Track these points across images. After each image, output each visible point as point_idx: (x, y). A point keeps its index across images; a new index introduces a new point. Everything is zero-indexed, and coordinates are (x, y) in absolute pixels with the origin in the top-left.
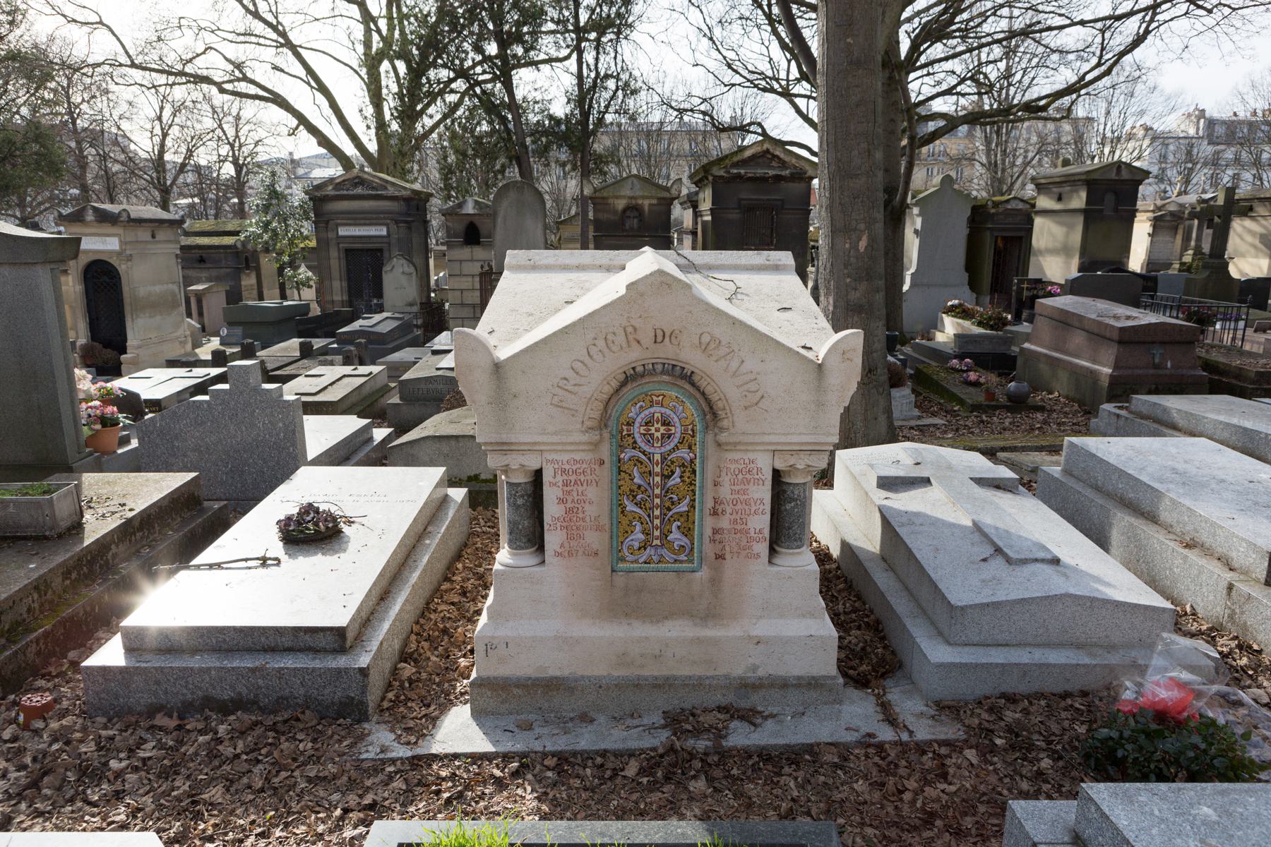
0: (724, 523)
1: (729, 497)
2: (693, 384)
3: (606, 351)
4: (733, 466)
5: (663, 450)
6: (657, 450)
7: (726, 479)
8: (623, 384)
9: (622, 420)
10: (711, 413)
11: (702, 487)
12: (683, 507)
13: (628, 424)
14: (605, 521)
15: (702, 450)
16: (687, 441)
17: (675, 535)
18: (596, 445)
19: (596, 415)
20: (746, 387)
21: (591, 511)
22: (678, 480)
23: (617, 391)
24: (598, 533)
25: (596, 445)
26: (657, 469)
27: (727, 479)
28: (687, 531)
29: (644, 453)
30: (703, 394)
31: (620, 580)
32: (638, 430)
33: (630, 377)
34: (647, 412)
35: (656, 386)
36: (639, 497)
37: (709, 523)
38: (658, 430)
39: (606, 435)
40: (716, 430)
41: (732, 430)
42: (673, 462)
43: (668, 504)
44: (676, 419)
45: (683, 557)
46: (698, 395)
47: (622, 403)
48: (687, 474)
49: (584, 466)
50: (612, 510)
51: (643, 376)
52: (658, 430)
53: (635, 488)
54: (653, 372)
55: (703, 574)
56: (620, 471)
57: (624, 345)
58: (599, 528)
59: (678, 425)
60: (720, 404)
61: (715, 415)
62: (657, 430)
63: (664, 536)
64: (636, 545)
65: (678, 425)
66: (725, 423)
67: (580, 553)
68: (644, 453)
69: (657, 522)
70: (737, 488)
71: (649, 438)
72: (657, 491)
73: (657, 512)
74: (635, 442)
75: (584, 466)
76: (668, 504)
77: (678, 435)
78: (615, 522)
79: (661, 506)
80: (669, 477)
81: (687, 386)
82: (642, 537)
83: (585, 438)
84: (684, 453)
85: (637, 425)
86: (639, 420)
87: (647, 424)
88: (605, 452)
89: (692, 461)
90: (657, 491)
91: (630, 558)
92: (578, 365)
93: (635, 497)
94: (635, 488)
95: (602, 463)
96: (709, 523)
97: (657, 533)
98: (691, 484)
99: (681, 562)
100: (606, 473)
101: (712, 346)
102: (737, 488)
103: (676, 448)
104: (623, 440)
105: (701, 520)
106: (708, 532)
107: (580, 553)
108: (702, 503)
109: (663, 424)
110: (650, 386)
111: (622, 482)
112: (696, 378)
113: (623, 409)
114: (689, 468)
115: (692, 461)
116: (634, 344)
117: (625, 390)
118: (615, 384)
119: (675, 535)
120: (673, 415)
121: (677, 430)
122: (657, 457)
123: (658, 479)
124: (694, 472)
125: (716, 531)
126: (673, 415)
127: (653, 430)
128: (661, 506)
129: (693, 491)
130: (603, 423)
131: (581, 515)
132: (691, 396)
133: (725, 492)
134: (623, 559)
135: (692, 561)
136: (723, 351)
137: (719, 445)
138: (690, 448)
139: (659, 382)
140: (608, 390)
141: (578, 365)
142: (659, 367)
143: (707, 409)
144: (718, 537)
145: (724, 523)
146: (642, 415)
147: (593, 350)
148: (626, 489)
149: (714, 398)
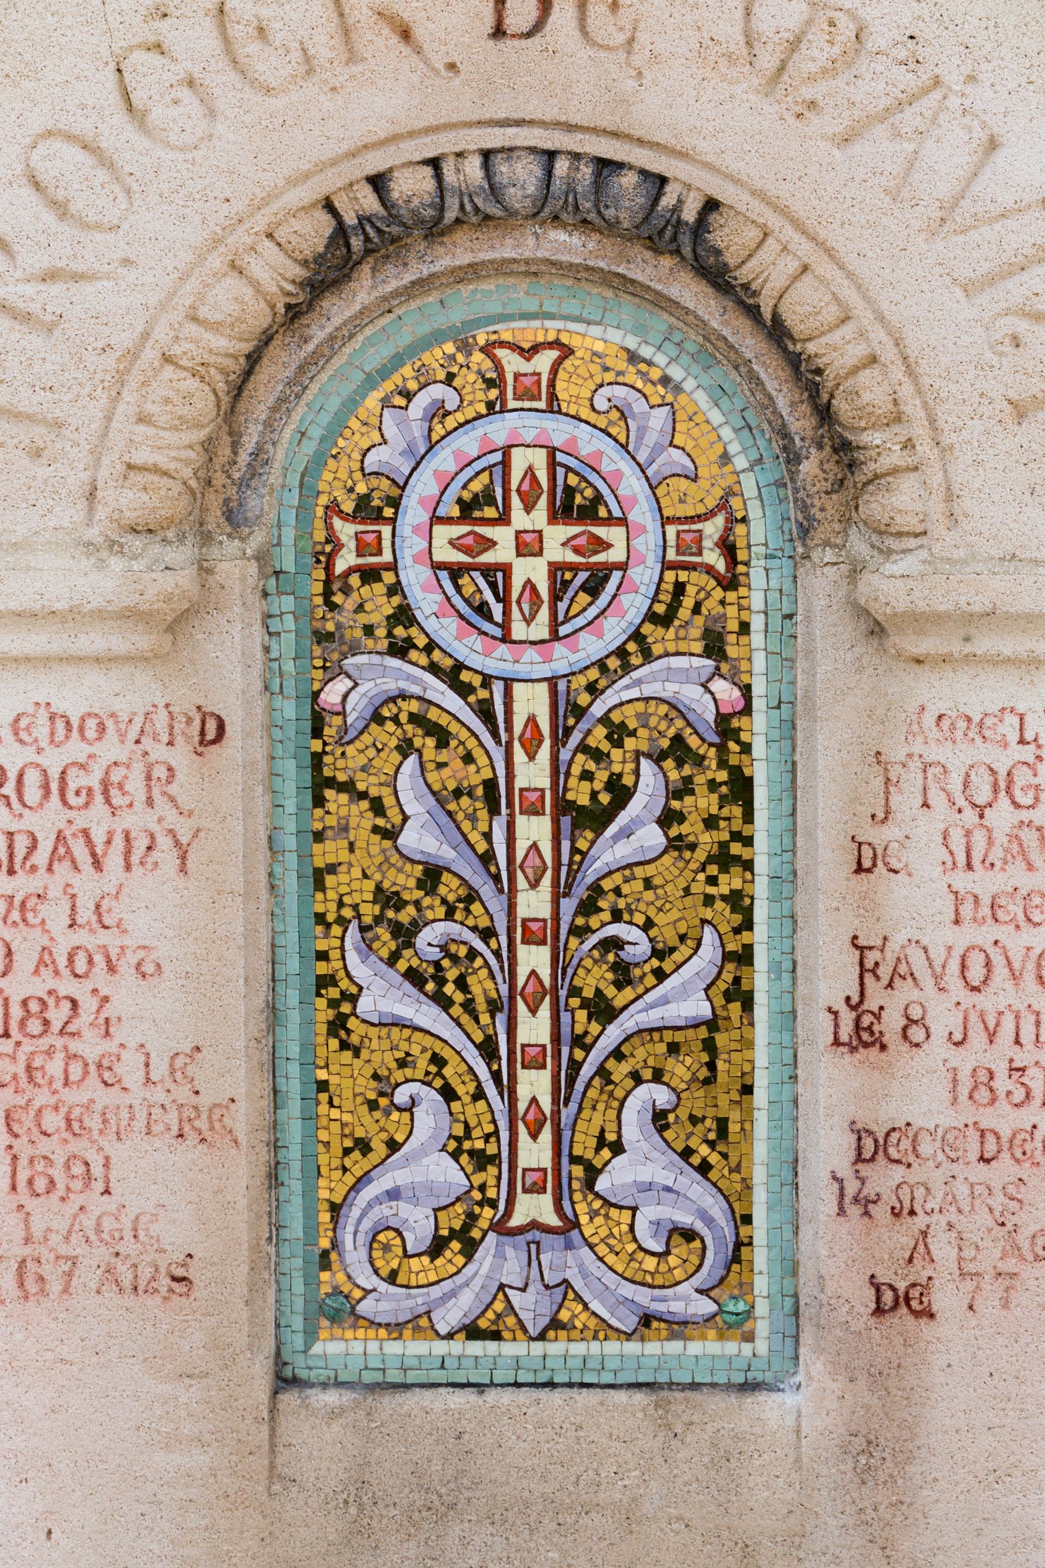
0: (918, 1092)
1: (943, 938)
2: (716, 275)
3: (221, 80)
4: (957, 757)
5: (563, 659)
6: (532, 664)
7: (919, 837)
8: (331, 269)
9: (336, 483)
10: (827, 443)
11: (788, 879)
12: (683, 999)
13: (366, 510)
14: (232, 1079)
15: (785, 660)
16: (696, 606)
17: (641, 1166)
18: (178, 624)
19: (174, 448)
20: (1016, 290)
21: (149, 1018)
22: (653, 837)
23: (294, 313)
24: (190, 1152)
25: (178, 624)
26: (533, 773)
27: (925, 830)
28: (710, 1142)
29: (453, 676)
30: (776, 332)
31: (320, 1434)
32: (418, 545)
33: (359, 243)
34: (468, 443)
35: (520, 294)
36: (428, 939)
37: (835, 1093)
38: (533, 546)
39: (235, 566)
40: (858, 544)
41: (945, 541)
42: (618, 733)
43: (595, 978)
44: (632, 485)
45: (687, 1301)
46: (750, 343)
47: (328, 390)
48: (705, 802)
49: (110, 750)
50: (273, 1012)
51: (435, 229)
52: (533, 546)
53: (404, 881)
54: (489, 212)
55: (806, 1406)
56: (320, 785)
57: (324, 45)
58: (196, 1126)
59: (643, 514)
60: (871, 391)
61: (845, 452)
62: (528, 545)
63: (578, 1172)
64: (419, 1224)
65: (643, 514)
66: (902, 501)
67: (88, 1276)
68: (453, 676)
69: (535, 1085)
70: (984, 883)
71: (484, 592)
72: (534, 903)
73: (534, 1028)
74: (404, 615)
75: (110, 750)
76: (595, 978)
77: (645, 575)
78: (293, 1087)
79: (558, 992)
80: (597, 818)
81: (689, 291)
82: (449, 1175)
83: (106, 583)
84: (679, 679)
85: (413, 513)
86: (424, 485)
87: (467, 509)
88: (232, 664)
89: (726, 727)
90: (534, 903)
91: (385, 1303)
92: (63, 163)
93: (405, 935)
94: (404, 881)
95: (213, 733)
96: (835, 1093)
97: (535, 1153)
98: (723, 859)
99: (679, 1327)
100: (237, 798)
101: (817, 52)
102: (984, 883)
103: (623, 659)
104: (337, 597)
105: (791, 1073)
106: (828, 1151)
107: (88, 1276)
108: (790, 969)
109: (564, 510)
110: (462, 305)
111: (331, 851)
112: (729, 238)
113: (338, 427)
114: (714, 765)
115: (726, 727)
116: (378, 42)
117: (338, 309)
118: (275, 273)
119: (641, 1166)
120: (614, 460)
121: (639, 549)
122: (532, 702)
123: (535, 830)
124: (741, 788)
125: (871, 1146)
126: (614, 460)
127: (504, 552)
128: (558, 992)
129: (739, 903)
130: (218, 496)
131: (90, 1046)
132: (713, 349)
133: (916, 908)
134: (342, 1311)
135: (736, 1325)
136: (877, 82)
137: (877, 630)
138: (714, 646)
139: (532, 270)
140: (240, 304)
141: (63, 163)
142: (522, 178)
143: (801, 424)
144: (883, 1179)
145: (918, 1092)
146: (444, 460)
147: (150, 77)
148: (353, 886)
149: (835, 352)
